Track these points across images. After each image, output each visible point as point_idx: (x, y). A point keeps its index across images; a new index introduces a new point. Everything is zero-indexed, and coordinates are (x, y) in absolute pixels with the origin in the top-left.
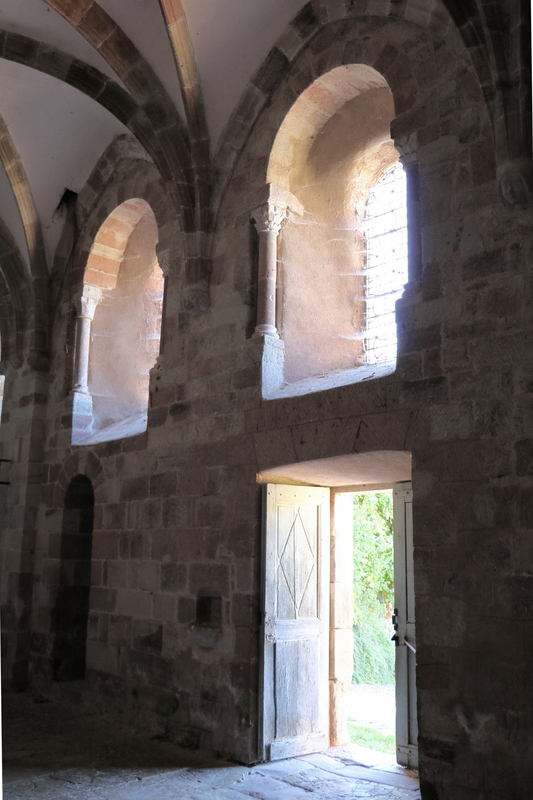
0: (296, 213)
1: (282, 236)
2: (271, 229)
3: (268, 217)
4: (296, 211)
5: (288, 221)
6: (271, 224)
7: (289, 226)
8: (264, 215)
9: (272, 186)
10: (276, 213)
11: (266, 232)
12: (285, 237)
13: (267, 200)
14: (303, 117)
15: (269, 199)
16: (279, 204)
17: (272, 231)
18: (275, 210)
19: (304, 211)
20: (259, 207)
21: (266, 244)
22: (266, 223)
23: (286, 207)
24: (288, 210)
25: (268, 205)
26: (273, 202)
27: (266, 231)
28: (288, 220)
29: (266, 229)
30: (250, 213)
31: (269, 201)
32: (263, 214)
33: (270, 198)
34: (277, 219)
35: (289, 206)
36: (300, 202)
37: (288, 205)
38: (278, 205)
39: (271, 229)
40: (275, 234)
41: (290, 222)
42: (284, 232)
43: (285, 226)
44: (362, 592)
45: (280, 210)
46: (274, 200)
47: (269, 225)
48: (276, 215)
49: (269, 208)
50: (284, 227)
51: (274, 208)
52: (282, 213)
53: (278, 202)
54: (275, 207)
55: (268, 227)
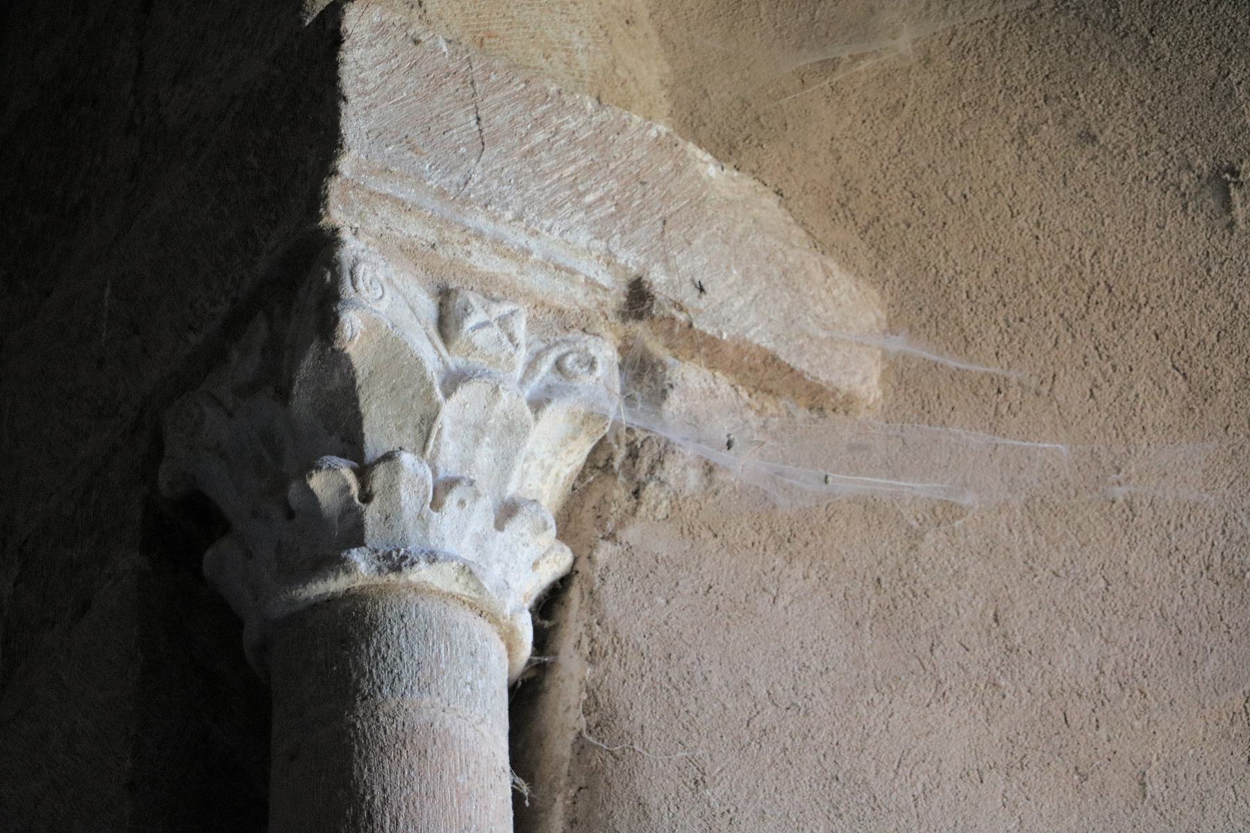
0: (771, 360)
1: (592, 658)
2: (396, 562)
3: (357, 419)
4: (761, 337)
5: (671, 470)
6: (392, 487)
7: (688, 532)
8: (302, 399)
9: (382, 29)
10: (455, 361)
11: (331, 601)
12: (634, 663)
13: (316, 202)
14: (630, 265)
15: (334, 188)
16: (498, 245)
17: (422, 573)
18: (446, 325)
19: (898, 344)
20: (235, 325)
21: (347, 753)
22: (317, 482)
23: (616, 296)
24: (640, 329)
25: (333, 265)
26: (414, 230)
27: (335, 585)
28: (667, 449)
29: (332, 561)
30: (158, 443)
31: (337, 214)
32: (283, 395)
33: (346, 164)
34: (480, 429)
35: (657, 278)
36: (819, 245)
37: (631, 260)
38: (484, 262)
39: (396, 562)
40: (464, 617)
41: (693, 478)
42: (612, 609)
43: (631, 534)
44: (451, 500)
45: (520, 328)
46: (408, 194)
47: (372, 513)
48: (454, 381)
49: (347, 289)
50: (605, 552)
51: (428, 306)
52: (559, 366)
53: (478, 220)
54: (444, 295)
55: (356, 537)
